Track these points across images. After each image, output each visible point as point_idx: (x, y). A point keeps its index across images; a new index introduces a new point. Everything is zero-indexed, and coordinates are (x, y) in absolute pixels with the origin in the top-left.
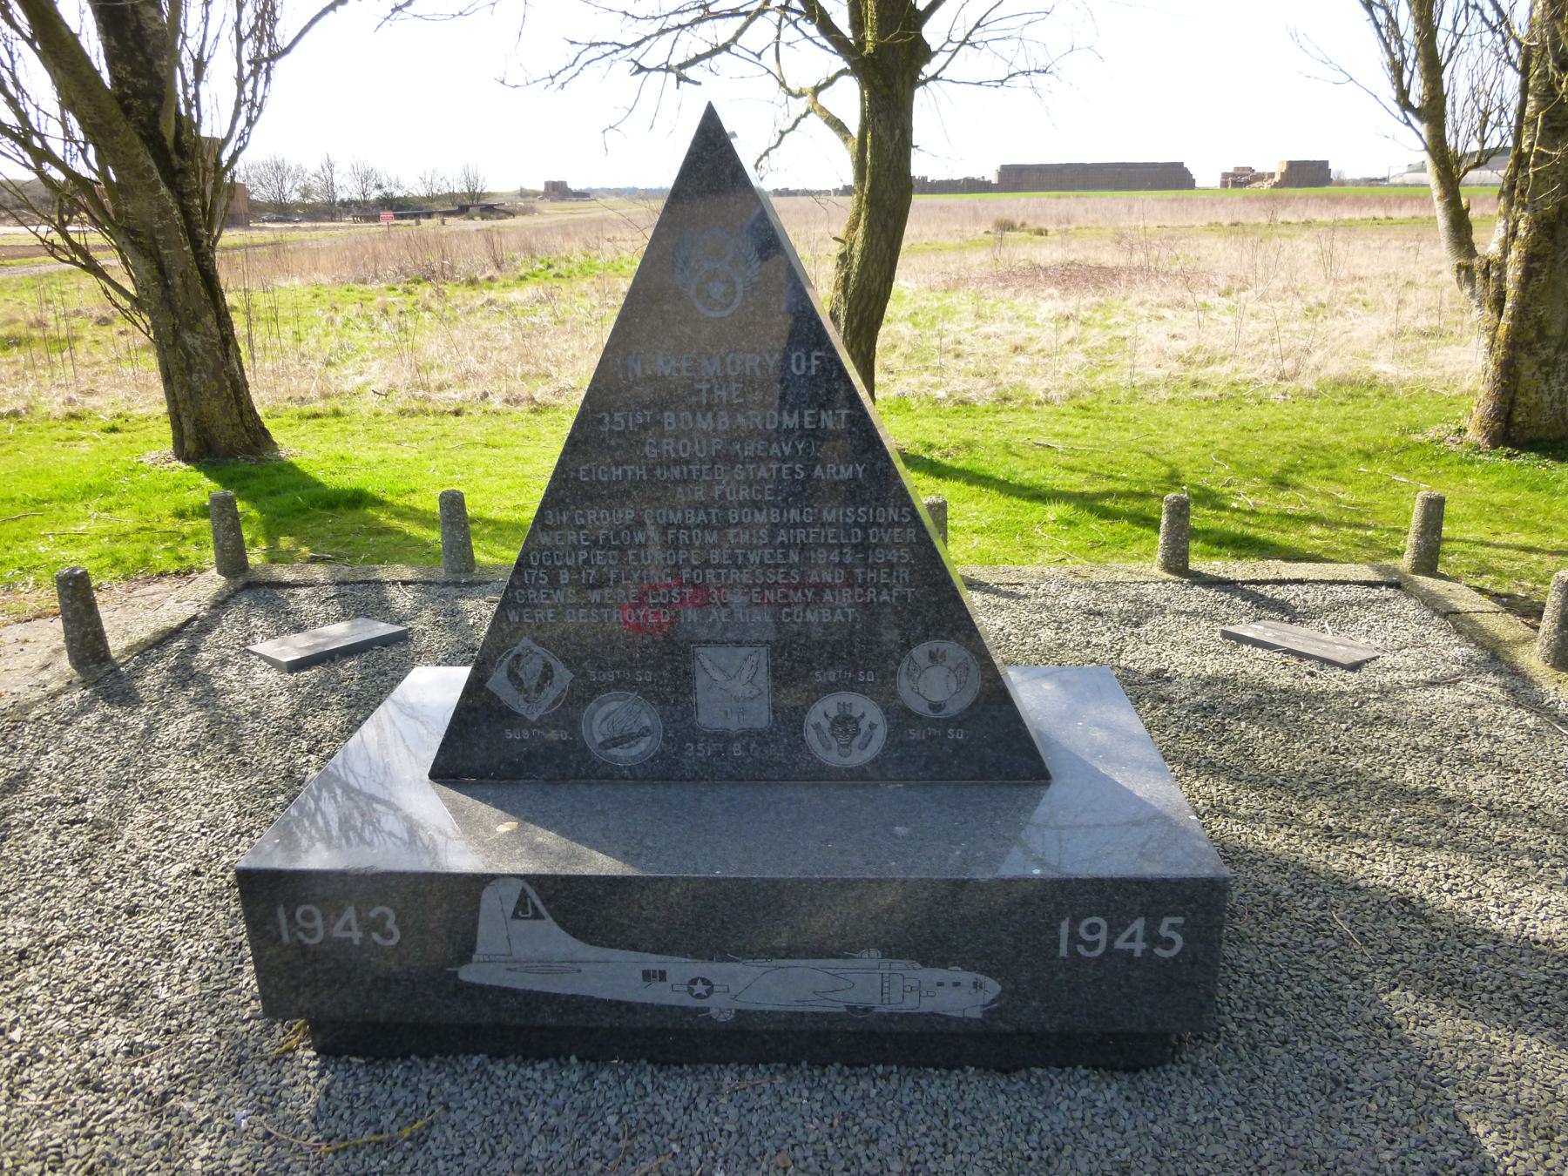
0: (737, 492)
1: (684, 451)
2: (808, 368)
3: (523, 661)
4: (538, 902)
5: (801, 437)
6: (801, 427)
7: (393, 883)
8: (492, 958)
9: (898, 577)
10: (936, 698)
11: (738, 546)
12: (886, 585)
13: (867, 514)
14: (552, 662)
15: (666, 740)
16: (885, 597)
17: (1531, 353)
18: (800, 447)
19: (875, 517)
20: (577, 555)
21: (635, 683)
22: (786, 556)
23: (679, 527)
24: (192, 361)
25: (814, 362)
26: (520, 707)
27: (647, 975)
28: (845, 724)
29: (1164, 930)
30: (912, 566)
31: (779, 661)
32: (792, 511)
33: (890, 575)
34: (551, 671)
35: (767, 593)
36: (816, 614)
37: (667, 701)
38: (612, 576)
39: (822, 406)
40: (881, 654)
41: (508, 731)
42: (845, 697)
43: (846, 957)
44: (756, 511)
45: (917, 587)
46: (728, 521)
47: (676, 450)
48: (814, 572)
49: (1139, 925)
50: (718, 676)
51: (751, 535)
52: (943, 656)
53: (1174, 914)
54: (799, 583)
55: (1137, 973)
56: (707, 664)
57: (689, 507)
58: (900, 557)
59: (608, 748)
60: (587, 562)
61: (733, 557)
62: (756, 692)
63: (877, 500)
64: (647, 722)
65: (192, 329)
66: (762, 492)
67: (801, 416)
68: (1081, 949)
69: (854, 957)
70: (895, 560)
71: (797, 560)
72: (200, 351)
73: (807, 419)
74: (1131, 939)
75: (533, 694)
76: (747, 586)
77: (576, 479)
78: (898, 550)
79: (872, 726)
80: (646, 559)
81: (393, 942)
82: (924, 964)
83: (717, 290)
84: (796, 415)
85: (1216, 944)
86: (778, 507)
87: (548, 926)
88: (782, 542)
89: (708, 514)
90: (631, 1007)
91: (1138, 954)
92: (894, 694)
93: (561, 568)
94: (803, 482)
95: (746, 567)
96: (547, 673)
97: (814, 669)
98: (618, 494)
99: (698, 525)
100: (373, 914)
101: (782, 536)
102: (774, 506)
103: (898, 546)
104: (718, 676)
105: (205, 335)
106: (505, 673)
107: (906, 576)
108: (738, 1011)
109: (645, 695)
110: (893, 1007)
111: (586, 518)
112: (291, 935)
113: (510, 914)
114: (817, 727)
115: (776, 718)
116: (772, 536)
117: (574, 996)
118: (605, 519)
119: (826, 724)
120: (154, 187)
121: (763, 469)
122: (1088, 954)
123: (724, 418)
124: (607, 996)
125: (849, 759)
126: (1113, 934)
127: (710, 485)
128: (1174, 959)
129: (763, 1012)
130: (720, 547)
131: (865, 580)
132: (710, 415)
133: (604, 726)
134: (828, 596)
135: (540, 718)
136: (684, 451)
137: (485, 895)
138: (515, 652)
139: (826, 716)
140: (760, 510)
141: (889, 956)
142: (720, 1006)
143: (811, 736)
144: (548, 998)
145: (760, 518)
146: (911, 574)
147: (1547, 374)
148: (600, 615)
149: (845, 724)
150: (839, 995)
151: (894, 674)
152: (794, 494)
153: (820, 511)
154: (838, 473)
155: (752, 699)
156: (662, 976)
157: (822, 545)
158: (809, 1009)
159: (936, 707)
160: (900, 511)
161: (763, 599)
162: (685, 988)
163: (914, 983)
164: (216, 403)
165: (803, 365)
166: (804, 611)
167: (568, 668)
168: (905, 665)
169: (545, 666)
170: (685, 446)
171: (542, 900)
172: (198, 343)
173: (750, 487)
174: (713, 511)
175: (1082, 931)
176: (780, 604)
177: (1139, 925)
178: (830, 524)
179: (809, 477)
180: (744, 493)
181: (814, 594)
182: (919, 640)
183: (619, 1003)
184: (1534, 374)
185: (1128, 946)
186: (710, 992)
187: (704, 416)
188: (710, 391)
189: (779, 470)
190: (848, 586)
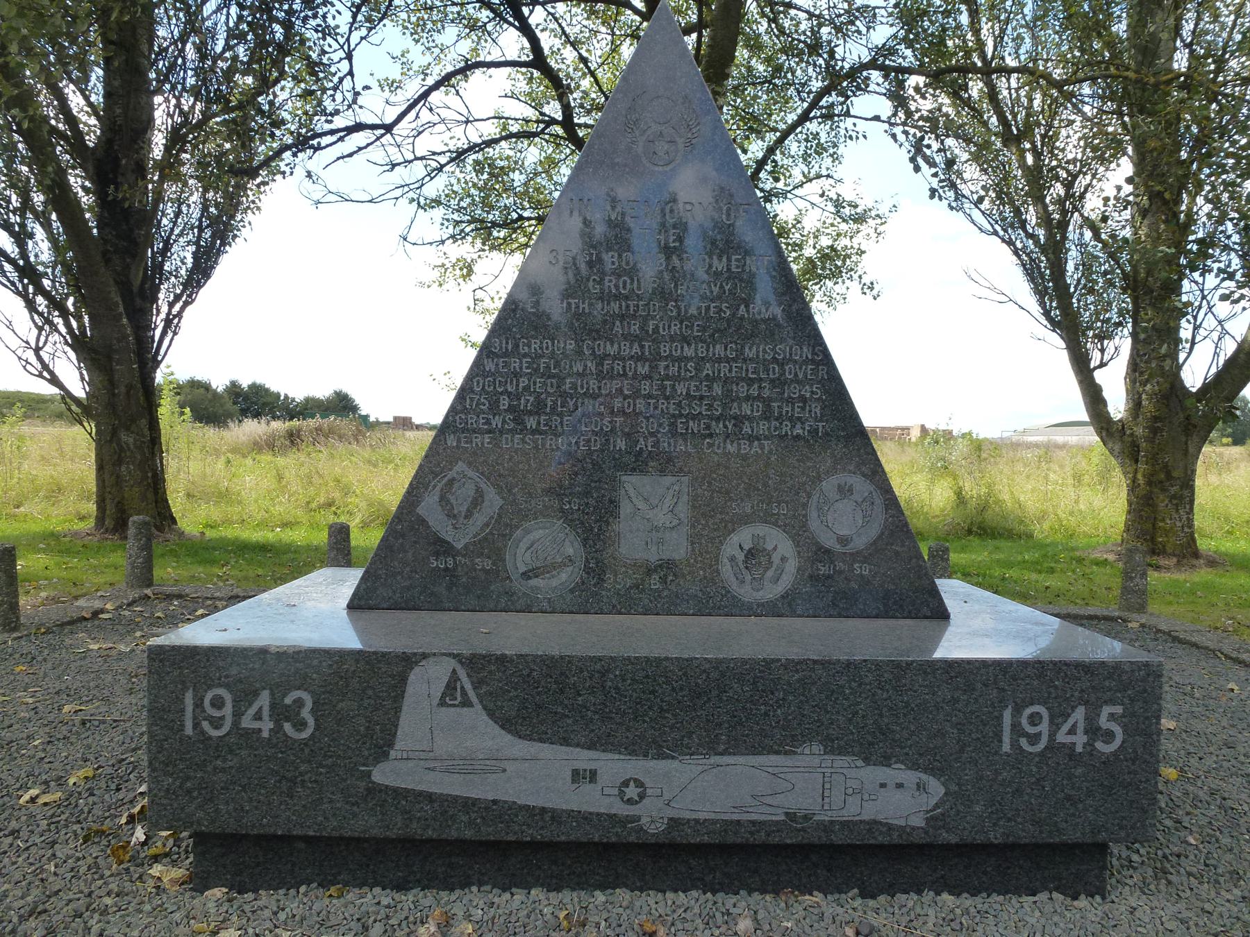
0: (670, 327)
1: (624, 288)
3: (456, 485)
4: (468, 687)
5: (728, 278)
6: (729, 270)
7: (315, 662)
8: (411, 755)
9: (810, 411)
10: (844, 532)
11: (667, 377)
12: (799, 419)
14: (483, 486)
15: (588, 570)
16: (798, 431)
17: (1164, 490)
18: (727, 288)
19: (791, 354)
20: (518, 381)
22: (710, 388)
23: (615, 358)
24: (123, 455)
26: (447, 534)
27: (576, 775)
29: (1103, 722)
30: (823, 401)
31: (700, 491)
32: (718, 346)
33: (803, 409)
34: (482, 496)
35: (691, 423)
36: (735, 444)
37: (592, 529)
38: (549, 403)
40: (793, 486)
42: (761, 529)
44: (685, 346)
45: (827, 421)
47: (616, 286)
48: (735, 404)
49: (1079, 714)
50: (641, 504)
51: (680, 368)
52: (851, 490)
53: (1111, 702)
54: (721, 414)
55: (1079, 771)
56: (632, 492)
57: (625, 339)
58: (812, 392)
59: (530, 578)
60: (527, 388)
61: (663, 388)
62: (676, 522)
64: (570, 551)
65: (128, 429)
67: (729, 260)
68: (1023, 742)
69: (795, 753)
70: (808, 395)
71: (720, 393)
72: (132, 446)
73: (734, 263)
74: (1072, 731)
76: (674, 416)
78: (811, 386)
79: (784, 559)
80: (582, 387)
81: (305, 735)
82: (867, 761)
84: (724, 259)
85: (1155, 737)
86: (705, 342)
87: (477, 716)
88: (708, 375)
89: (642, 347)
90: (556, 816)
91: (1079, 749)
92: (804, 526)
93: (501, 393)
94: (728, 321)
95: (673, 397)
96: (478, 500)
99: (632, 357)
100: (288, 701)
101: (708, 370)
102: (701, 341)
103: (811, 382)
104: (641, 504)
105: (137, 434)
106: (436, 498)
107: (818, 411)
108: (671, 819)
110: (835, 814)
111: (529, 347)
112: (196, 725)
113: (436, 701)
114: (732, 559)
115: (693, 550)
117: (495, 802)
118: (547, 348)
119: (741, 557)
120: (118, 318)
122: (1030, 749)
124: (531, 802)
125: (761, 593)
126: (1055, 726)
127: (645, 320)
128: (1115, 754)
129: (697, 821)
130: (651, 378)
131: (780, 414)
133: (528, 554)
134: (747, 429)
135: (466, 546)
136: (624, 288)
137: (414, 676)
138: (449, 477)
140: (689, 344)
141: (832, 752)
144: (469, 804)
145: (689, 352)
146: (822, 409)
147: (1177, 505)
148: (535, 442)
151: (805, 506)
152: (719, 331)
153: (743, 347)
157: (743, 379)
158: (745, 817)
159: (844, 541)
160: (814, 350)
161: (687, 429)
162: (616, 792)
163: (855, 784)
164: (137, 489)
166: (725, 441)
167: (499, 494)
168: (815, 498)
169: (477, 490)
170: (625, 283)
171: (472, 683)
172: (131, 440)
173: (681, 323)
175: (1024, 721)
176: (702, 435)
177: (1079, 714)
179: (734, 315)
180: (675, 329)
181: (734, 425)
182: (828, 473)
184: (1167, 505)
186: (642, 796)
187: (720, 260)
189: (708, 308)
190: (765, 419)
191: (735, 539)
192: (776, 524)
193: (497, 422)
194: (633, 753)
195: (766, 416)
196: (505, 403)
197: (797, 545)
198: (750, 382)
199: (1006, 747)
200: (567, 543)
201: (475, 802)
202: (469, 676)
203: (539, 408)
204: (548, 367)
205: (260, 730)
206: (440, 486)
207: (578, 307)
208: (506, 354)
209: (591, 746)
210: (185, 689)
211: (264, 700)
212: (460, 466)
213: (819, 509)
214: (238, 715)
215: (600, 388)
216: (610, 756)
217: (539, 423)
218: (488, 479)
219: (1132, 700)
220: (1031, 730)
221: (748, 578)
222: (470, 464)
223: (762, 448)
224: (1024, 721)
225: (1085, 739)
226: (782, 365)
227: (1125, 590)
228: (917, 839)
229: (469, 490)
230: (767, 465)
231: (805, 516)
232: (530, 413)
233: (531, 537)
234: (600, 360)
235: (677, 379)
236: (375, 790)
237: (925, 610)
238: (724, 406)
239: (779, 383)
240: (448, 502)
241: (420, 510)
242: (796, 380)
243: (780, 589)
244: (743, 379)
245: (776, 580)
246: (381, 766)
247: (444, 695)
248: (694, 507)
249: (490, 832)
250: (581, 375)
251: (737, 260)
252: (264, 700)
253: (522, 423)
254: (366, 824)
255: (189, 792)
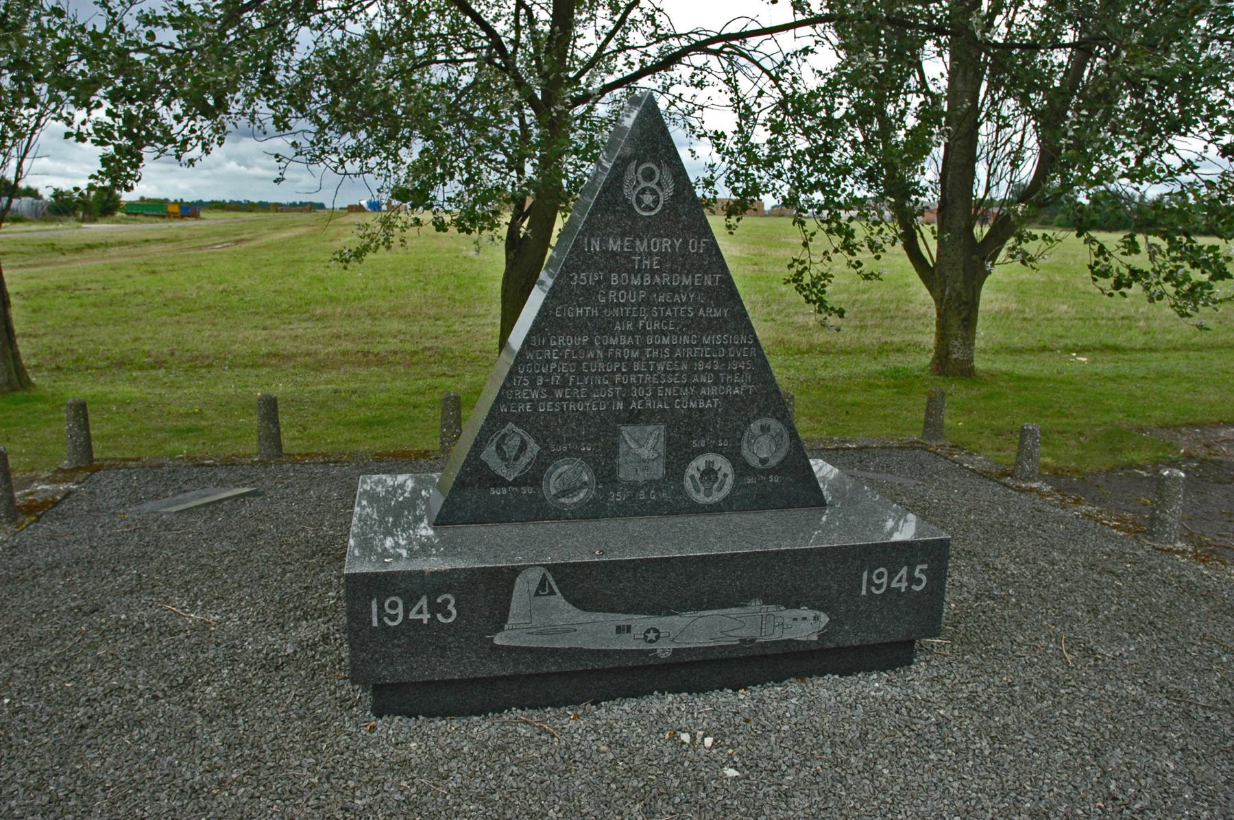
1: (622, 298)
2: (699, 248)
4: (553, 583)
6: (693, 284)
11: (651, 359)
13: (728, 338)
15: (598, 490)
18: (692, 296)
21: (581, 452)
22: (679, 365)
23: (616, 347)
25: (703, 245)
26: (502, 471)
27: (619, 629)
28: (709, 473)
29: (917, 574)
33: (740, 377)
37: (600, 463)
39: (705, 272)
41: (492, 489)
42: (711, 457)
43: (742, 606)
46: (645, 343)
47: (617, 297)
50: (633, 445)
52: (769, 428)
53: (922, 563)
55: (902, 602)
61: (648, 366)
62: (656, 455)
63: (735, 329)
64: (586, 478)
66: (667, 324)
67: (693, 277)
68: (873, 589)
73: (696, 280)
75: (511, 462)
76: (655, 385)
77: (554, 315)
78: (745, 361)
81: (450, 620)
82: (787, 607)
83: (648, 199)
87: (558, 599)
89: (634, 339)
90: (606, 653)
92: (739, 454)
93: (538, 374)
94: (692, 319)
96: (523, 447)
97: (693, 439)
98: (579, 327)
100: (439, 600)
103: (745, 359)
104: (633, 445)
106: (494, 448)
108: (674, 649)
109: (586, 460)
112: (380, 620)
114: (692, 477)
116: (672, 353)
117: (569, 649)
119: (697, 476)
121: (669, 310)
122: (877, 592)
123: (648, 278)
126: (891, 579)
127: (637, 320)
132: (639, 276)
134: (703, 392)
135: (515, 479)
139: (698, 470)
140: (666, 336)
142: (664, 649)
143: (688, 484)
144: (554, 652)
145: (666, 341)
149: (709, 473)
150: (736, 633)
151: (740, 440)
152: (686, 326)
153: (702, 337)
154: (713, 313)
155: (653, 460)
156: (629, 629)
157: (701, 358)
159: (763, 461)
165: (696, 246)
170: (623, 294)
171: (555, 581)
173: (661, 322)
174: (637, 337)
177: (904, 572)
178: (707, 345)
179: (696, 315)
180: (657, 325)
182: (755, 418)
183: (599, 651)
185: (898, 585)
186: (658, 637)
187: (687, 277)
188: (640, 261)
191: (694, 464)
192: (721, 453)
193: (535, 395)
194: (653, 613)
195: (716, 383)
196: (540, 381)
197: (734, 466)
198: (706, 360)
199: (864, 592)
200: (584, 473)
201: (557, 650)
202: (553, 577)
203: (564, 383)
204: (570, 355)
205: (422, 620)
206: (496, 439)
207: (590, 312)
208: (541, 347)
209: (627, 612)
210: (371, 599)
211: (424, 602)
212: (510, 425)
213: (748, 442)
214: (407, 611)
215: (605, 368)
216: (639, 616)
217: (564, 393)
218: (530, 433)
219: (933, 561)
220: (877, 582)
221: (702, 489)
222: (517, 424)
223: (713, 403)
224: (874, 577)
225: (906, 584)
226: (726, 347)
227: (927, 424)
228: (813, 647)
229: (516, 441)
230: (716, 414)
231: (740, 447)
232: (558, 387)
233: (559, 471)
234: (606, 349)
235: (658, 360)
236: (495, 648)
237: (812, 502)
238: (689, 377)
239: (725, 360)
240: (502, 449)
241: (483, 457)
242: (736, 358)
243: (722, 495)
244: (701, 358)
245: (720, 489)
246: (499, 635)
247: (538, 590)
248: (668, 445)
249: (568, 667)
250: (594, 359)
251: (699, 277)
252: (424, 602)
253: (553, 394)
254: (494, 668)
255: (377, 660)
